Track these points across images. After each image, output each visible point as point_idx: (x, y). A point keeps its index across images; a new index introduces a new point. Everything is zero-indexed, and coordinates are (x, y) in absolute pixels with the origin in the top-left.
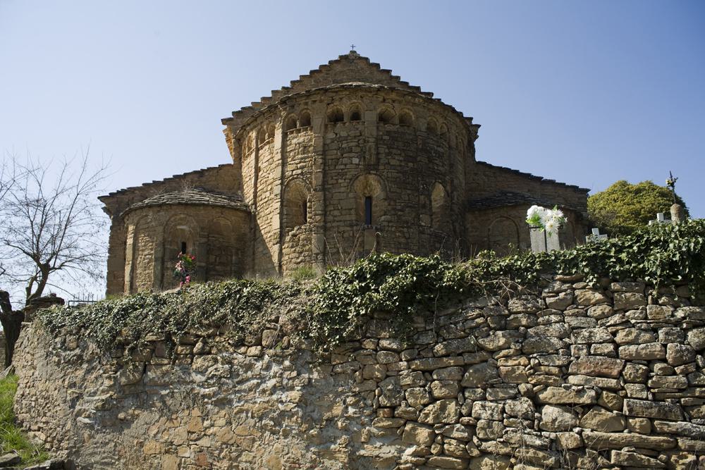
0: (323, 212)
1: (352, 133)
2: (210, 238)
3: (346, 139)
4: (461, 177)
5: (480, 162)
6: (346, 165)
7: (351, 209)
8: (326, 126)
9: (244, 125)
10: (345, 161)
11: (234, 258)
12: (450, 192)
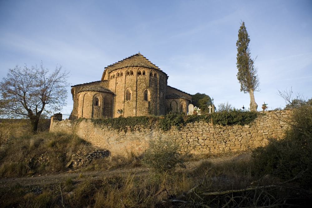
1: (144, 78)
5: (168, 86)
9: (110, 68)
10: (142, 85)
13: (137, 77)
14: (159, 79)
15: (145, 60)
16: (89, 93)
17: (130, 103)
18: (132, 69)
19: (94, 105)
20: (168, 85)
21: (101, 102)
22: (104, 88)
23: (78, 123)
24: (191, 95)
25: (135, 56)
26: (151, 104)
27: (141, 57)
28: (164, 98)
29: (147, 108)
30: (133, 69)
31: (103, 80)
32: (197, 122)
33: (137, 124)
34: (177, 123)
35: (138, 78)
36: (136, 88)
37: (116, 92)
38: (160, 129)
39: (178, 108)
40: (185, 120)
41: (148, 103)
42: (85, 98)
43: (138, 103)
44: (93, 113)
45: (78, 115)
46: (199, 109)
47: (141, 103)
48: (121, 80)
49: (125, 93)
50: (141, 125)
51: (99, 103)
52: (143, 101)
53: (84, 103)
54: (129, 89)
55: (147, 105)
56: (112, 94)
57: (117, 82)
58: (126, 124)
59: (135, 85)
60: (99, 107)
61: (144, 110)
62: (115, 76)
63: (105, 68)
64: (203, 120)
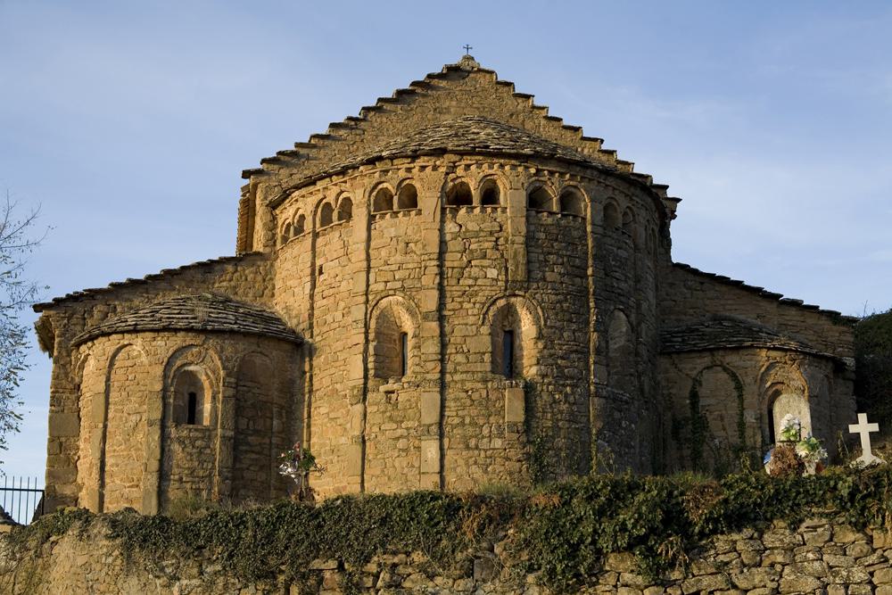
0: (440, 357)
1: (487, 226)
2: (239, 388)
3: (476, 235)
4: (651, 295)
5: (678, 265)
6: (476, 279)
7: (484, 353)
8: (443, 210)
9: (275, 178)
10: (475, 271)
11: (275, 422)
12: (634, 323)
13: (443, 221)
14: (603, 221)
15: (511, 104)
16: (138, 344)
17: (403, 397)
18: (409, 170)
19: (170, 423)
20: (677, 256)
21: (214, 398)
22: (244, 305)
23: (46, 546)
24: (850, 321)
25: (443, 83)
26: (545, 396)
27: (483, 81)
28: (643, 350)
29: (512, 426)
30: (415, 171)
31: (246, 255)
32: (782, 524)
33: (383, 545)
34: (642, 540)
35: (450, 227)
36: (436, 293)
38: (531, 578)
39: (750, 418)
40: (693, 517)
41: (520, 392)
43: (451, 394)
44: (163, 475)
45: (80, 488)
46: (870, 421)
47: (476, 396)
48: (342, 250)
49: (367, 333)
50: (408, 554)
51: (207, 407)
52: (485, 381)
54: (395, 304)
55: (514, 409)
56: (285, 340)
57: (318, 263)
58: (315, 550)
59: (430, 279)
60: (207, 429)
61: (498, 443)
62: (308, 226)
63: (246, 174)
64: (831, 507)
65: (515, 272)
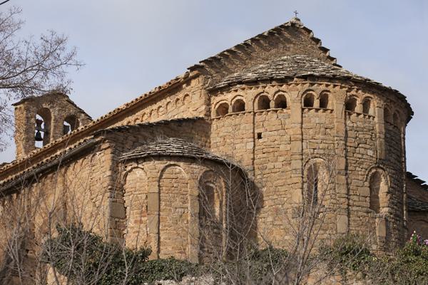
10: (362, 151)
20: (407, 171)
21: (221, 204)
37: (257, 172)
42: (165, 182)
43: (352, 218)
52: (368, 212)
53: (163, 203)
65: (381, 154)
